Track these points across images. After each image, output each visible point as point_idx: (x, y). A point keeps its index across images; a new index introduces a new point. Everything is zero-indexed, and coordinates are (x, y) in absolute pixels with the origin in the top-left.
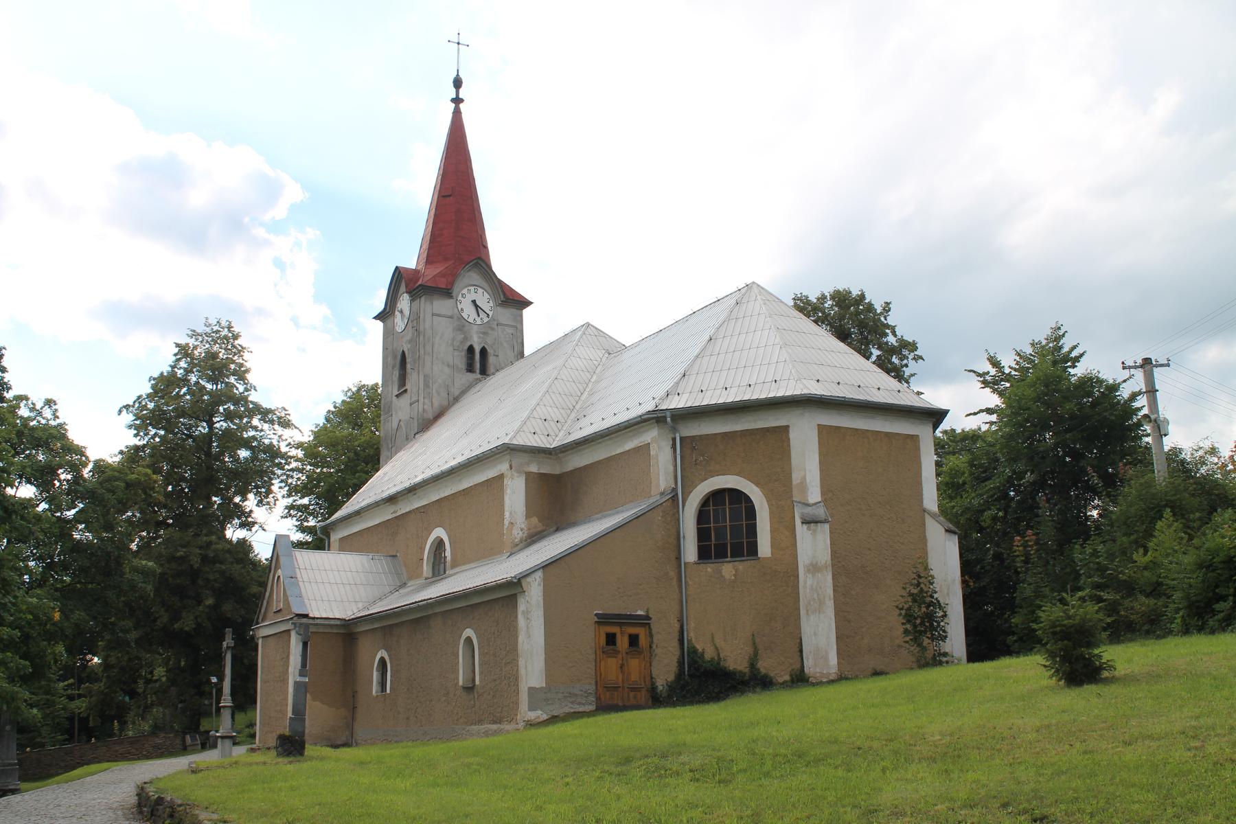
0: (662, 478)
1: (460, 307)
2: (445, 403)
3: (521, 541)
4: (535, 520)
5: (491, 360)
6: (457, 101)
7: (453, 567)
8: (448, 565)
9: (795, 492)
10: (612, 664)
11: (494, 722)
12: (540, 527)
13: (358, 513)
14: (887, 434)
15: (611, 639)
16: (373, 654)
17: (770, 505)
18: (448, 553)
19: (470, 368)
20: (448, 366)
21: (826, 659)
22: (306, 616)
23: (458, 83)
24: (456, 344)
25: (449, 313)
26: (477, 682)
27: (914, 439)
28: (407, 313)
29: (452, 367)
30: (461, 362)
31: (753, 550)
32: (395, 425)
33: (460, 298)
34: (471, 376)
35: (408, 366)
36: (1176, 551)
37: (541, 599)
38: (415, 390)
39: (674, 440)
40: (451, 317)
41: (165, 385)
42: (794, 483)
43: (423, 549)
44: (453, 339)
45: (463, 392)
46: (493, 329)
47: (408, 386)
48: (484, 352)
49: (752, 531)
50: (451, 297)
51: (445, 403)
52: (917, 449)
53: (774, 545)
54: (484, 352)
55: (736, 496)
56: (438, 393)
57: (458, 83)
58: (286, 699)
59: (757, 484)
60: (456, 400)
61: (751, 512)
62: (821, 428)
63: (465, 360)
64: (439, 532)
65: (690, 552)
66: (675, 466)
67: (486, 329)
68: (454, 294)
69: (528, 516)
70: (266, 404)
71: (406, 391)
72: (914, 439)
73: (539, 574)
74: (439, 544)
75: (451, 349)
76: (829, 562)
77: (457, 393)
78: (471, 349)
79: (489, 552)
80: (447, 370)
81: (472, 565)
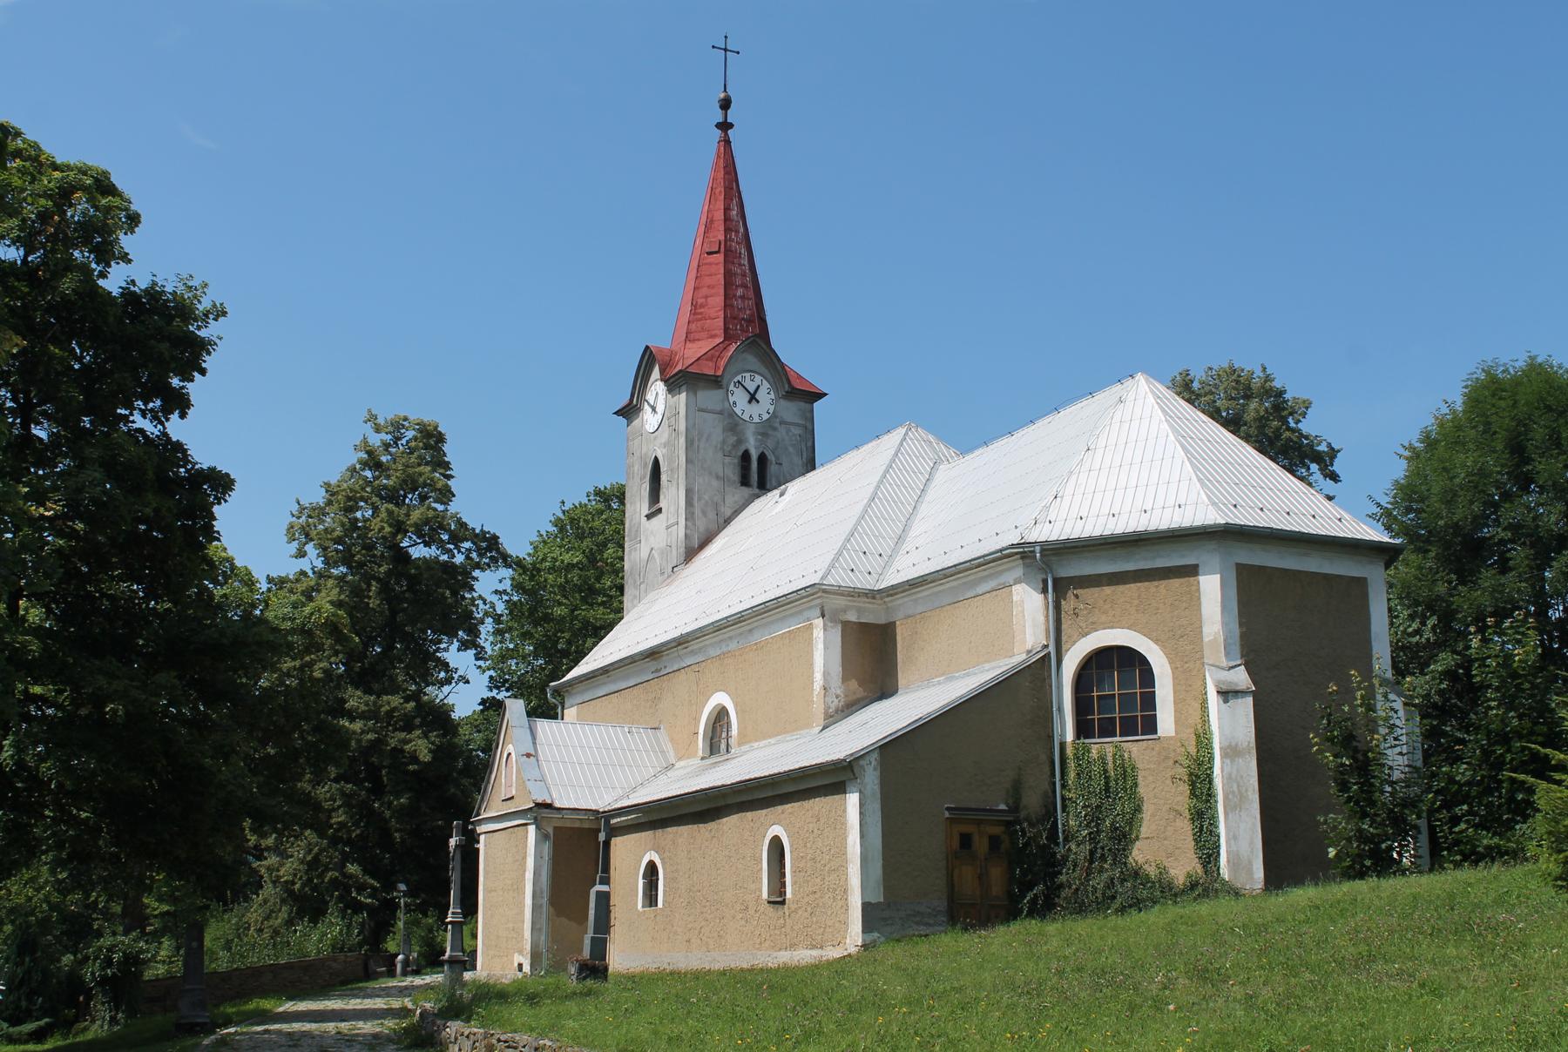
0: (1029, 631)
1: (732, 399)
2: (714, 527)
3: (837, 711)
4: (854, 684)
5: (772, 469)
6: (725, 126)
7: (740, 744)
8: (732, 742)
9: (1207, 652)
10: (967, 874)
11: (814, 947)
12: (860, 693)
13: (605, 671)
14: (1326, 576)
15: (966, 841)
16: (630, 856)
17: (1174, 669)
18: (734, 731)
19: (745, 481)
20: (718, 477)
21: (1250, 872)
22: (549, 806)
23: (726, 104)
24: (728, 448)
25: (718, 408)
26: (789, 895)
27: (1361, 583)
28: (660, 408)
29: (722, 479)
30: (733, 474)
31: (1150, 726)
32: (644, 554)
33: (731, 387)
34: (746, 491)
35: (664, 478)
36: (1499, 901)
37: (877, 788)
38: (672, 509)
39: (1045, 582)
40: (721, 413)
41: (345, 499)
42: (1206, 639)
43: (697, 720)
44: (724, 442)
45: (736, 513)
46: (775, 429)
47: (663, 504)
48: (762, 459)
49: (1149, 701)
50: (720, 387)
51: (714, 527)
52: (1364, 597)
53: (1178, 722)
54: (762, 459)
55: (1128, 660)
56: (704, 513)
57: (726, 104)
58: (522, 913)
59: (1156, 641)
60: (728, 521)
61: (1148, 677)
62: (1238, 565)
63: (738, 470)
64: (721, 698)
65: (1067, 728)
66: (1047, 616)
67: (767, 428)
68: (725, 382)
69: (845, 679)
70: (474, 523)
71: (660, 510)
72: (1361, 583)
73: (876, 755)
74: (721, 715)
75: (720, 455)
76: (1253, 744)
77: (728, 513)
78: (746, 456)
79: (786, 725)
80: (715, 483)
81: (772, 741)
